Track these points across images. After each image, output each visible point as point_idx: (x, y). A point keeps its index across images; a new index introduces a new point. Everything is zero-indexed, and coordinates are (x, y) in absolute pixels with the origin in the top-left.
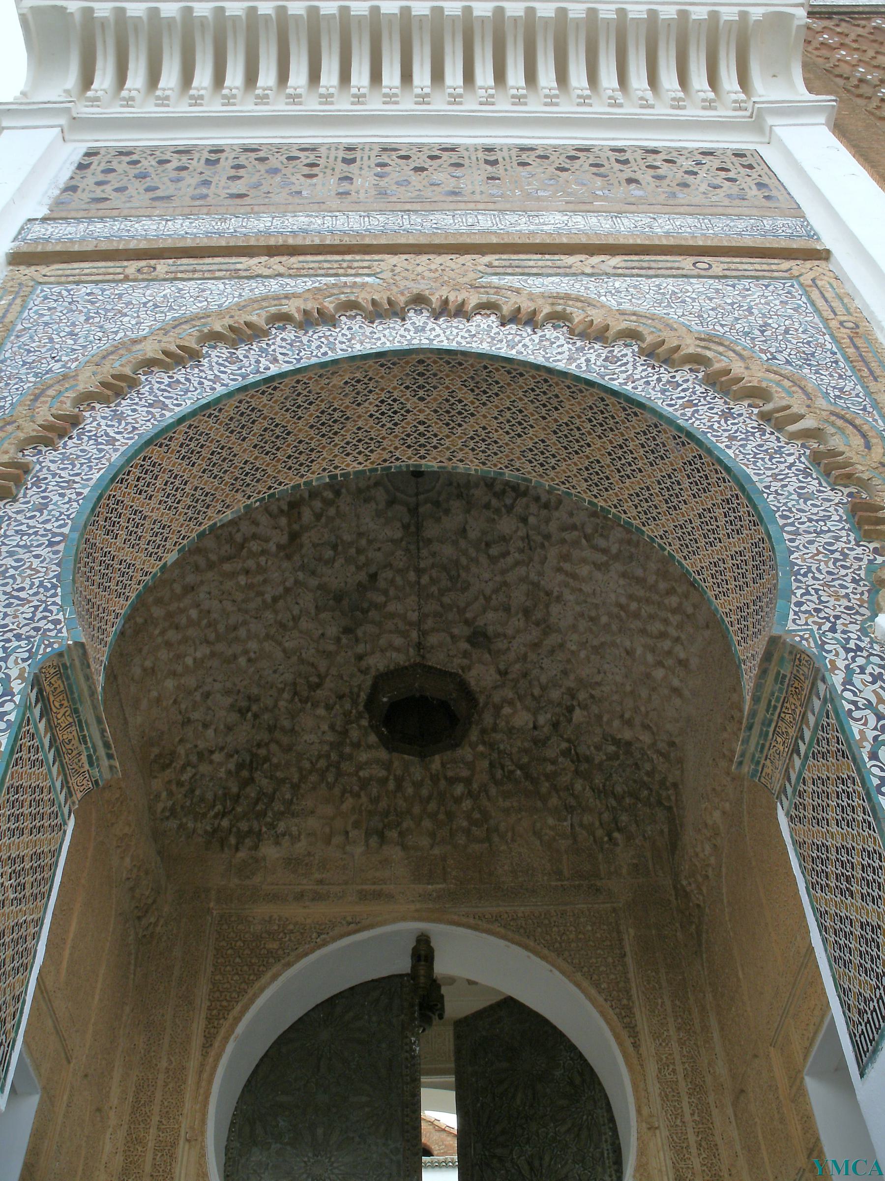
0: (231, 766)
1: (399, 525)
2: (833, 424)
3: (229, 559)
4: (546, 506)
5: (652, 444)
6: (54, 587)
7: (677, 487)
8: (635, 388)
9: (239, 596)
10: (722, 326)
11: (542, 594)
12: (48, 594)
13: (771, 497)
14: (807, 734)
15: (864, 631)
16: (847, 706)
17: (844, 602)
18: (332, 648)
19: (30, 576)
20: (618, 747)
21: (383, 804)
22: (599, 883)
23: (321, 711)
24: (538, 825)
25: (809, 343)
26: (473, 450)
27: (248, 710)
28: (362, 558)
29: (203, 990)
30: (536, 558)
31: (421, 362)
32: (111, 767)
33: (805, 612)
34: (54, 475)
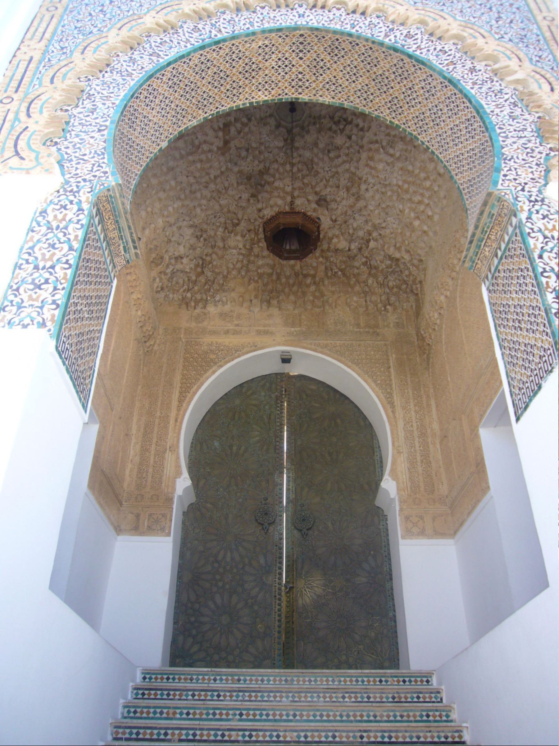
0: (192, 266)
1: (282, 139)
2: (533, 77)
3: (191, 154)
4: (362, 130)
5: (428, 87)
6: (103, 154)
7: (440, 113)
8: (421, 53)
9: (197, 175)
10: (474, 18)
11: (357, 178)
12: (100, 157)
13: (494, 117)
14: (503, 246)
15: (540, 191)
16: (528, 230)
17: (531, 176)
18: (244, 205)
19: (89, 148)
20: (392, 262)
21: (270, 287)
22: (378, 331)
23: (239, 238)
24: (349, 300)
25: (524, 29)
26: (328, 90)
27: (201, 236)
28: (262, 157)
29: (178, 378)
30: (355, 159)
31: (301, 35)
32: (136, 254)
33: (508, 180)
34: (99, 93)
